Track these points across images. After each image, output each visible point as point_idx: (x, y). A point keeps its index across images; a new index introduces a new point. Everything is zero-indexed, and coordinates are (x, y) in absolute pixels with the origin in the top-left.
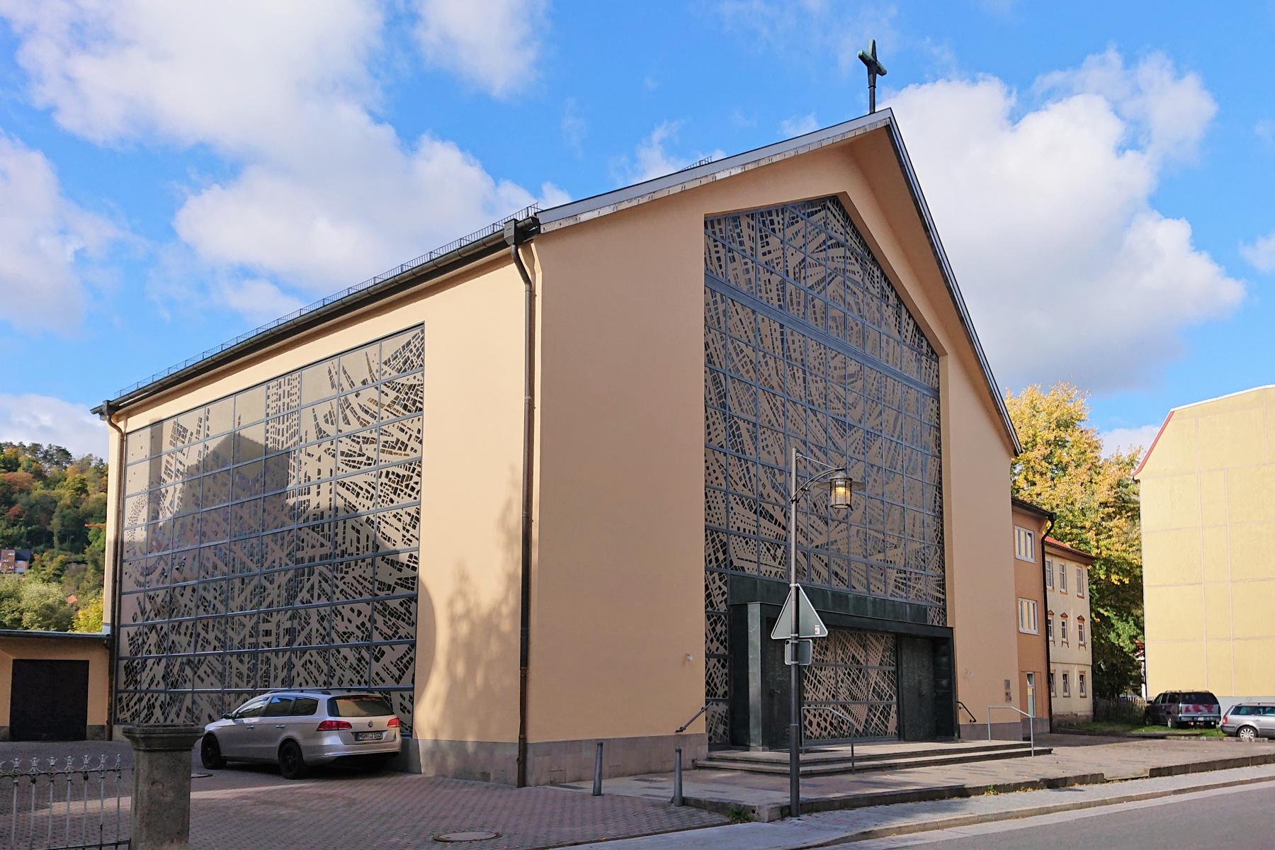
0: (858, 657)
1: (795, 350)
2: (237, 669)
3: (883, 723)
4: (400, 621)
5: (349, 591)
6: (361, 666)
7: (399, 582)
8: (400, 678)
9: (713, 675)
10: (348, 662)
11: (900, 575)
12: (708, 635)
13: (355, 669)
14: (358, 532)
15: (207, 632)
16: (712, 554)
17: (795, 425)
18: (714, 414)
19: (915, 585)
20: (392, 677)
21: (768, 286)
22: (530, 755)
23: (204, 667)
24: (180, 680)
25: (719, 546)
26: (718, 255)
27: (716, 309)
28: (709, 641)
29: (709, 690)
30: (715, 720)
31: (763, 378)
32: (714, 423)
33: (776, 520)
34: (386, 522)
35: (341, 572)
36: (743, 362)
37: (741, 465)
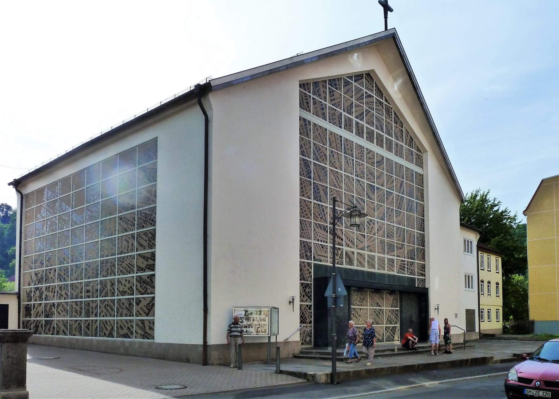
0: (380, 303)
1: (348, 149)
2: (75, 308)
3: (392, 335)
4: (148, 286)
5: (124, 271)
6: (131, 307)
7: (147, 266)
8: (149, 313)
9: (304, 313)
10: (125, 305)
11: (402, 263)
12: (302, 293)
13: (128, 309)
14: (128, 242)
15: (61, 291)
16: (304, 253)
17: (348, 187)
18: (305, 182)
19: (410, 267)
20: (145, 313)
21: (334, 117)
22: (209, 351)
23: (60, 308)
24: (50, 314)
25: (308, 249)
26: (307, 101)
27: (306, 128)
28: (302, 296)
29: (302, 320)
30: (305, 335)
31: (331, 163)
32: (305, 186)
33: (338, 236)
34: (140, 237)
35: (121, 262)
36: (320, 155)
37: (320, 208)
